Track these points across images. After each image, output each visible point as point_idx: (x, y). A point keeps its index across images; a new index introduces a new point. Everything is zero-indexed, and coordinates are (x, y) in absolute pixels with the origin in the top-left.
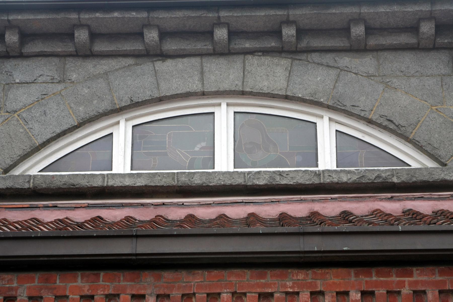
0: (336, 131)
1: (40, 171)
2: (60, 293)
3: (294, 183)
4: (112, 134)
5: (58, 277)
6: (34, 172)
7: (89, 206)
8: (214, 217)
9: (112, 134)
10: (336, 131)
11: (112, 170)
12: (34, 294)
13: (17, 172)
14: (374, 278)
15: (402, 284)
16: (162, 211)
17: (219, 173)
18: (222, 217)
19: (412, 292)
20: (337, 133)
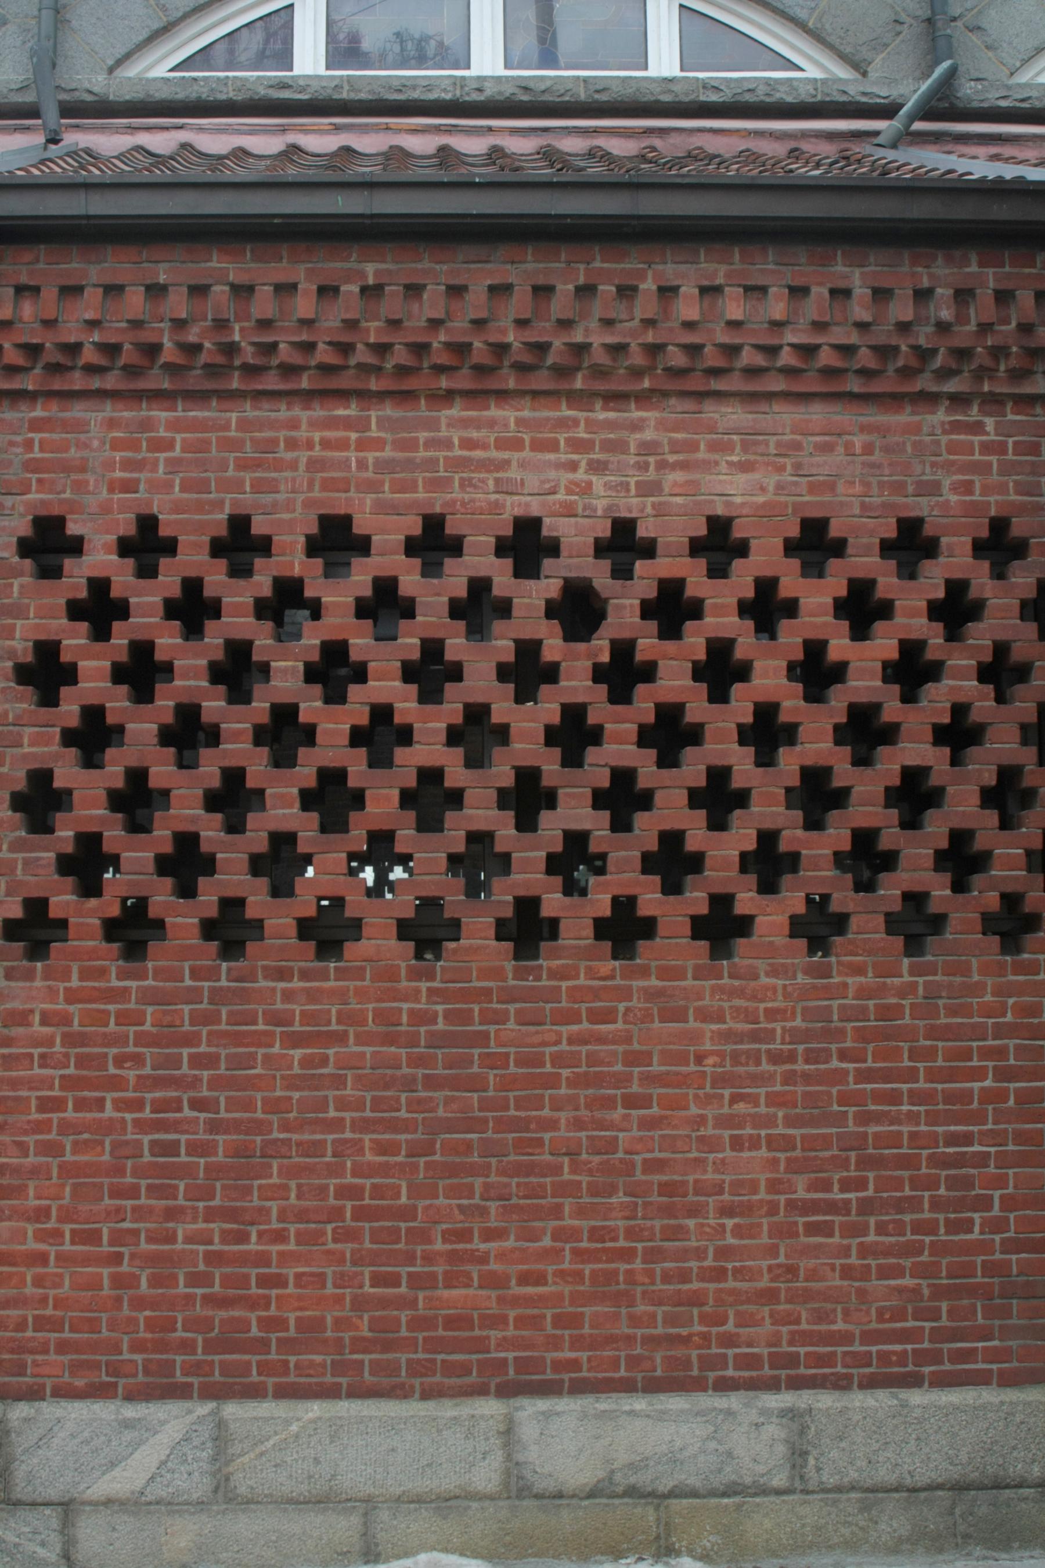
0: (681, 6)
1: (171, 70)
2: (842, 284)
3: (864, 94)
4: (292, 5)
5: (839, 253)
6: (161, 71)
7: (438, 129)
8: (224, 151)
9: (292, 5)
10: (681, 6)
11: (646, 68)
12: (541, 281)
13: (132, 71)
14: (1007, 269)
15: (642, 276)
16: (601, 142)
17: (299, 77)
18: (348, 151)
19: (869, 291)
20: (684, 10)
